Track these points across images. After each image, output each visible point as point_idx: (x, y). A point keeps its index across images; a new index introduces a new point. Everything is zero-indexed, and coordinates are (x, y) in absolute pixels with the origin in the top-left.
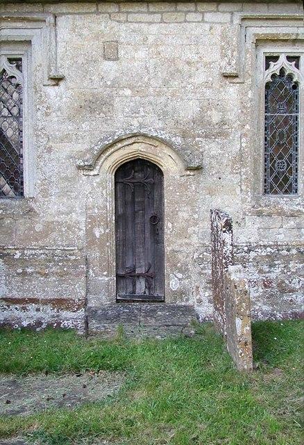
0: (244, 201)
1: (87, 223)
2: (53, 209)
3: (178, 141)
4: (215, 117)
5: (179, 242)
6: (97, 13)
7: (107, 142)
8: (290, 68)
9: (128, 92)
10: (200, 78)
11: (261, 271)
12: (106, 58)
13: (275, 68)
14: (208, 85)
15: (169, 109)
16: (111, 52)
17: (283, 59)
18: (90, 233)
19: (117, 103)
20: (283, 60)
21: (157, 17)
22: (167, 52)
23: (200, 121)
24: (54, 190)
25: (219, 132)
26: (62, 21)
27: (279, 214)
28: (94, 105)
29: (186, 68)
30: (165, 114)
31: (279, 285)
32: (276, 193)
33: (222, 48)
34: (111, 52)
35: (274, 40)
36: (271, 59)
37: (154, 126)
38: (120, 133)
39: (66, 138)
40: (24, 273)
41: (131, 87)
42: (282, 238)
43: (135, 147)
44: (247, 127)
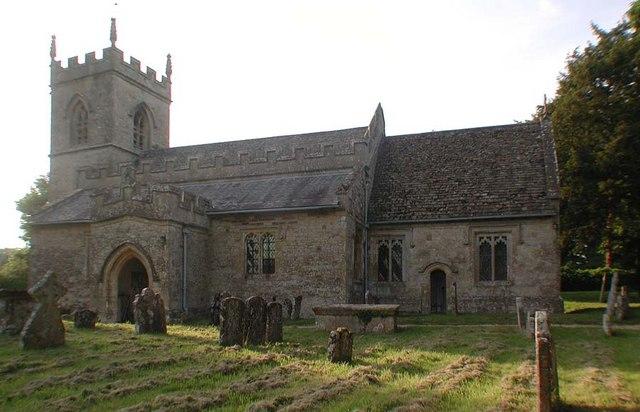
8: (503, 240)
16: (429, 238)
25: (464, 261)
28: (425, 253)
34: (429, 238)
35: (481, 233)
36: (481, 238)
37: (443, 260)
39: (416, 263)
42: (485, 294)
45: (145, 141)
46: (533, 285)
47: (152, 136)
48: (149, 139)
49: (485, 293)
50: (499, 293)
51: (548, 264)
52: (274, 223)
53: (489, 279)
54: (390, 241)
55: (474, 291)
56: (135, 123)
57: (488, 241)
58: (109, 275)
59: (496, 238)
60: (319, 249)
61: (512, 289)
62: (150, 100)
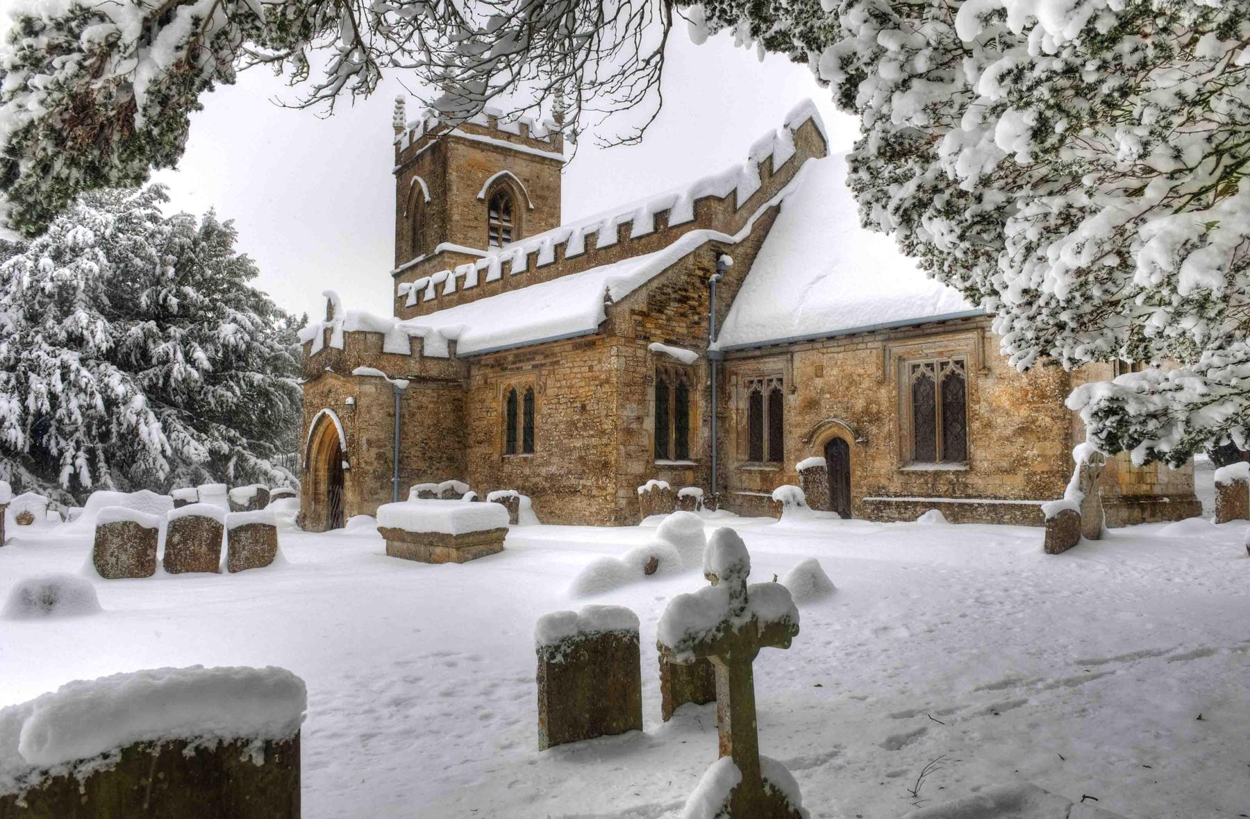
0: (892, 464)
4: (874, 408)
10: (865, 385)
12: (817, 376)
16: (819, 371)
17: (951, 363)
20: (922, 369)
22: (849, 369)
23: (866, 411)
25: (876, 419)
30: (848, 408)
39: (798, 425)
41: (830, 393)
46: (1011, 471)
60: (583, 407)
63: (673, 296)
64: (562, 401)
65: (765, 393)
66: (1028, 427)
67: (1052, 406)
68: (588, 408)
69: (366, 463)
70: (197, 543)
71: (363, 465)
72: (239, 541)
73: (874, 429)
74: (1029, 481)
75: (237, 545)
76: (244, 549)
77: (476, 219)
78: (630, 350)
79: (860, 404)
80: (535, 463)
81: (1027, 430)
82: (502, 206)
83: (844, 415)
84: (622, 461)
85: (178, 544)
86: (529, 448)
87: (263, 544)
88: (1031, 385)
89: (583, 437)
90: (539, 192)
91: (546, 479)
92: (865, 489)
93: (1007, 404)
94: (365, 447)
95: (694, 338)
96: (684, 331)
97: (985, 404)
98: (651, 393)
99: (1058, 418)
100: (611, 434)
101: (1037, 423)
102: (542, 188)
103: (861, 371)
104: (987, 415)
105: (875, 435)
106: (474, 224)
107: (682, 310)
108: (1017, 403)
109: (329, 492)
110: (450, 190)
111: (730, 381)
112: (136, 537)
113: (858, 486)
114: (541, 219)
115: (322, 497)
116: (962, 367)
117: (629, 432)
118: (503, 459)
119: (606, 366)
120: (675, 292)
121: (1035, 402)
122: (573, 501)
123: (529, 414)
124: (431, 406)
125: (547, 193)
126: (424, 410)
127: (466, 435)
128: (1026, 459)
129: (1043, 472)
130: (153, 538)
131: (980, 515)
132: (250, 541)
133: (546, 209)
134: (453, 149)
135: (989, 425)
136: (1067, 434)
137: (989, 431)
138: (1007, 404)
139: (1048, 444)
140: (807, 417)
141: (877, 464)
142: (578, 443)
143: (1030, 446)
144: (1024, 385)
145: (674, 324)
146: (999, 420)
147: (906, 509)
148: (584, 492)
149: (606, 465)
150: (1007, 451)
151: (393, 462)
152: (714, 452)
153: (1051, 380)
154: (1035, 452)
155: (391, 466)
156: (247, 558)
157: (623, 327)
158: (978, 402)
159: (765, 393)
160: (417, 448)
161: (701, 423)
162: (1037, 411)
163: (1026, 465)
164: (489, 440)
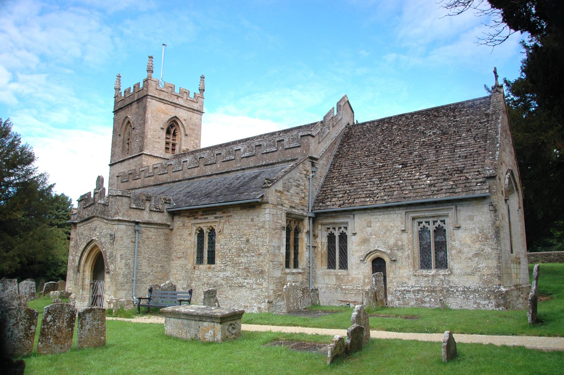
0: (410, 271)
1: (363, 278)
2: (354, 273)
3: (389, 252)
4: (400, 243)
5: (390, 284)
6: (365, 213)
7: (278, 165)
8: (442, 224)
9: (374, 237)
11: (415, 296)
12: (368, 227)
13: (421, 226)
14: (397, 233)
15: (386, 241)
17: (439, 221)
18: (364, 281)
19: (371, 240)
20: (424, 223)
21: (382, 213)
23: (396, 245)
24: (354, 268)
25: (401, 248)
26: (356, 216)
27: (421, 276)
29: (391, 228)
30: (385, 243)
31: (421, 300)
32: (424, 268)
33: (401, 221)
35: (419, 218)
36: (420, 223)
38: (372, 250)
39: (357, 251)
40: (345, 293)
41: (375, 235)
42: (423, 285)
43: (377, 254)
44: (410, 246)
45: (177, 147)
46: (472, 274)
47: (183, 143)
48: (180, 144)
49: (423, 283)
50: (437, 283)
51: (488, 250)
52: (216, 218)
53: (334, 268)
54: (337, 229)
55: (412, 282)
56: (168, 132)
57: (426, 225)
58: (84, 267)
59: (434, 222)
60: (248, 241)
61: (452, 278)
62: (182, 114)
63: (293, 184)
64: (233, 237)
65: (337, 234)
66: (480, 253)
67: (491, 243)
68: (250, 241)
69: (119, 268)
70: (61, 321)
71: (118, 270)
72: (85, 319)
73: (400, 254)
74: (481, 279)
75: (83, 322)
76: (87, 324)
77: (159, 138)
78: (275, 211)
79: (392, 241)
80: (215, 270)
81: (479, 254)
82: (172, 132)
83: (384, 246)
84: (271, 270)
85: (50, 322)
86: (211, 260)
87: (98, 321)
88: (481, 233)
89: (247, 257)
90: (191, 127)
91: (223, 279)
92: (395, 284)
93: (469, 242)
94: (119, 259)
95: (302, 205)
96: (298, 201)
97: (458, 242)
98: (284, 233)
99: (495, 249)
100: (265, 255)
101: (484, 251)
102: (193, 125)
103: (392, 225)
104: (459, 247)
105: (400, 257)
106: (158, 140)
107: (297, 191)
108: (474, 242)
109: (91, 284)
110: (147, 122)
111: (318, 228)
112: (25, 318)
113: (391, 282)
114: (191, 140)
115: (86, 287)
116: (444, 223)
117: (275, 255)
118: (194, 268)
119: (262, 219)
120: (295, 181)
121: (482, 241)
122: (240, 291)
123: (212, 243)
124: (154, 237)
125: (194, 127)
126: (150, 239)
127: (170, 254)
128: (479, 268)
129: (488, 275)
130: (35, 318)
131: (457, 296)
132: (91, 319)
133: (194, 135)
134: (150, 102)
135: (460, 252)
136: (499, 257)
137: (460, 255)
138: (469, 242)
139: (490, 261)
140: (363, 247)
141: (401, 271)
142: (244, 260)
143: (481, 262)
144: (477, 233)
145: (294, 198)
146: (465, 250)
147: (418, 293)
148: (248, 286)
149: (262, 272)
150: (470, 265)
151: (133, 268)
152: (311, 265)
153: (490, 231)
154: (484, 265)
155: (132, 270)
156: (89, 330)
157: (272, 198)
158: (455, 241)
159: (337, 234)
160: (145, 261)
161: (305, 249)
162: (484, 245)
163: (479, 271)
164: (185, 256)
